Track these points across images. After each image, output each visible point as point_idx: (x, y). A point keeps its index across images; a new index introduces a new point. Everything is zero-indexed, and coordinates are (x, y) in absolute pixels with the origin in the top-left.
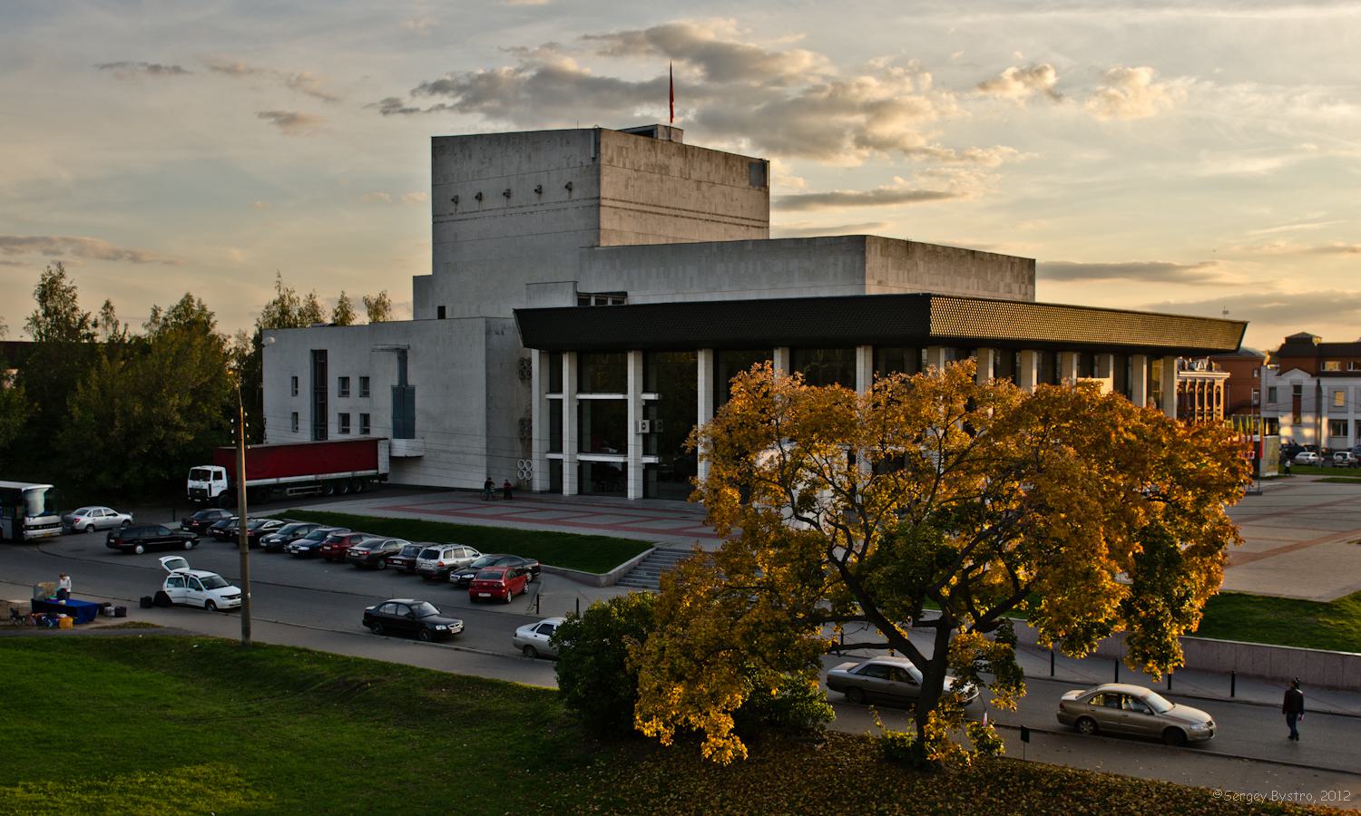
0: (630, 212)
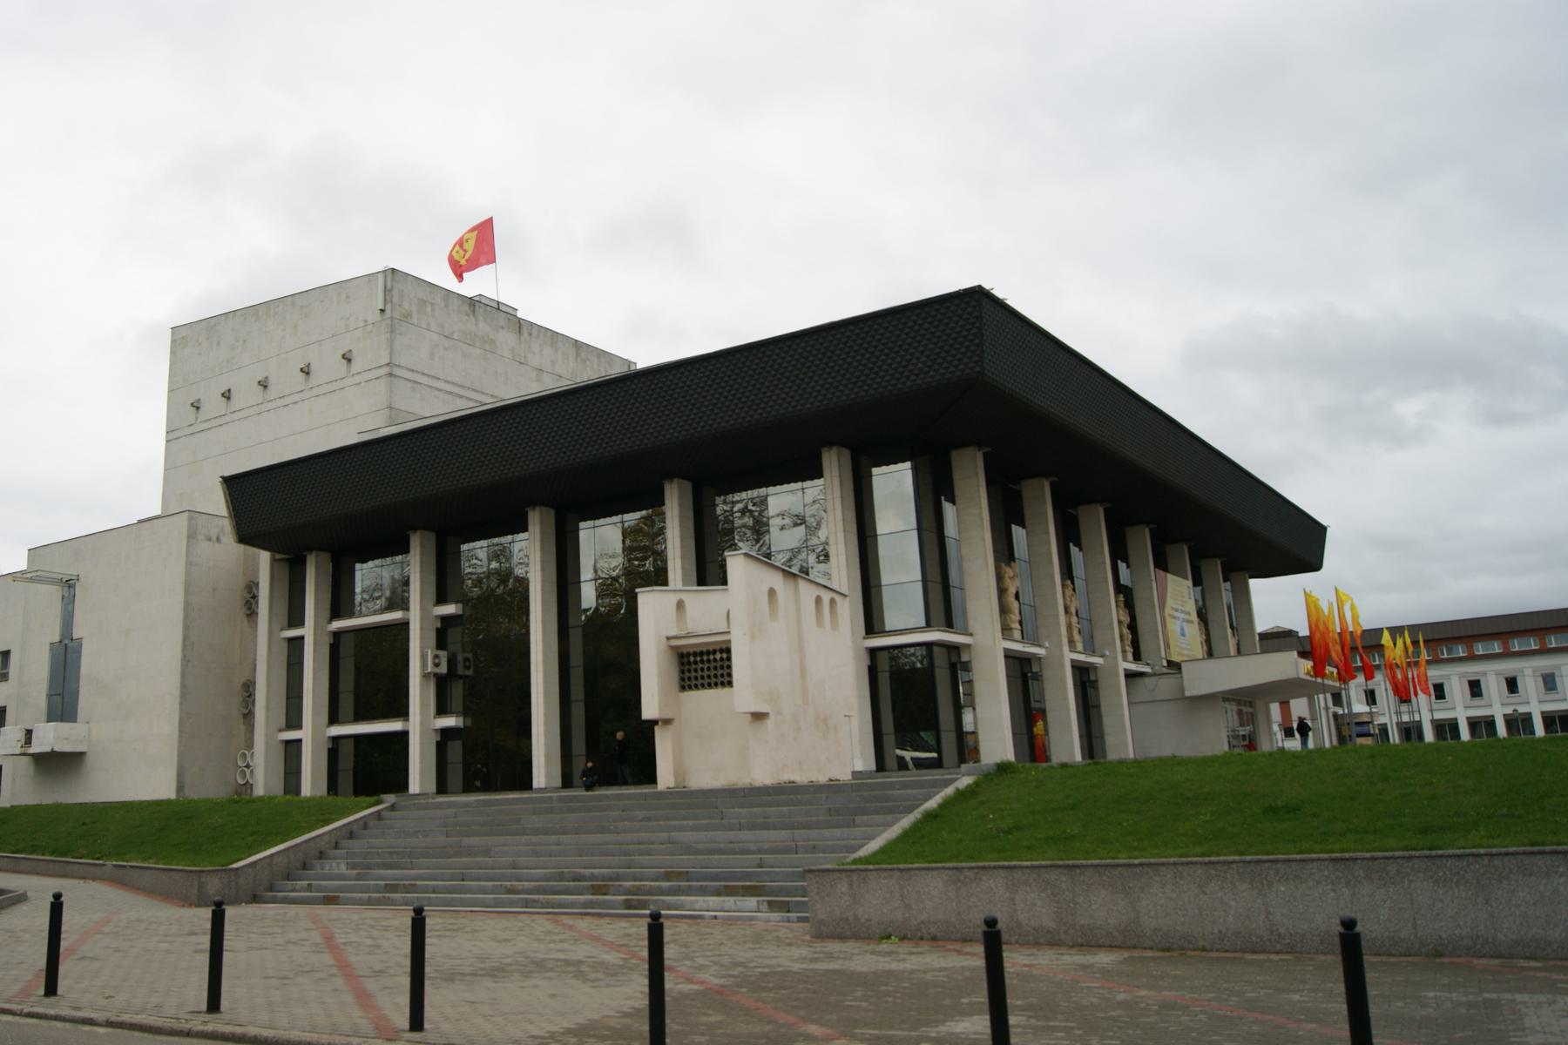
0: (437, 393)
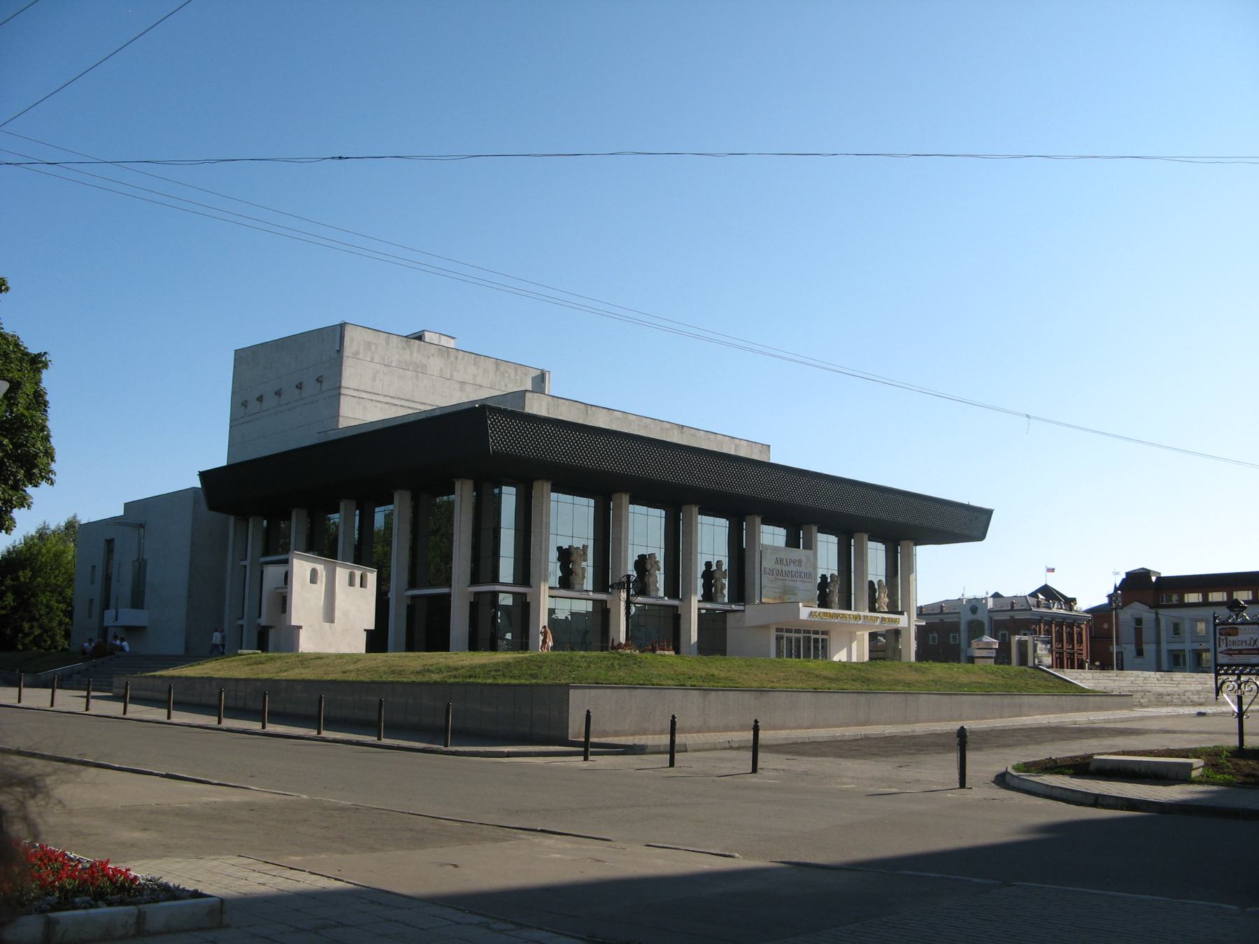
0: (377, 403)
